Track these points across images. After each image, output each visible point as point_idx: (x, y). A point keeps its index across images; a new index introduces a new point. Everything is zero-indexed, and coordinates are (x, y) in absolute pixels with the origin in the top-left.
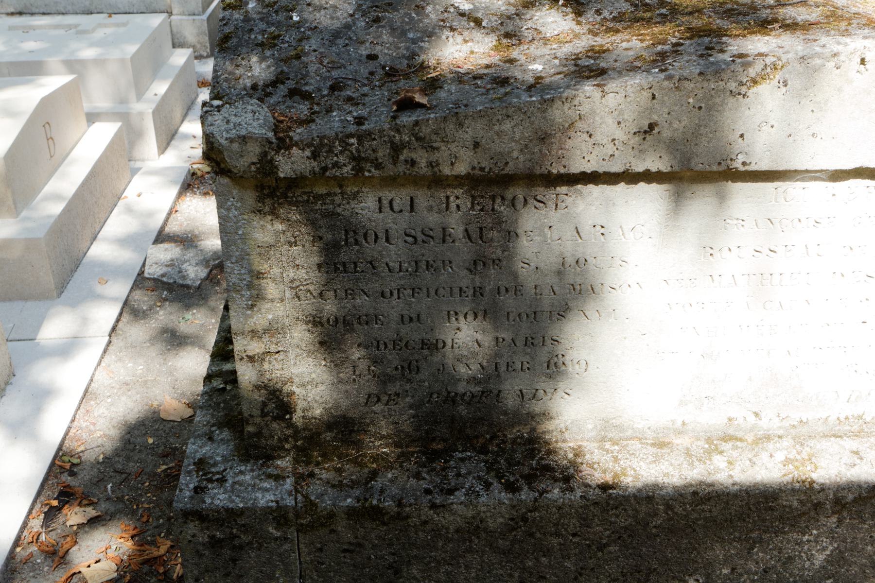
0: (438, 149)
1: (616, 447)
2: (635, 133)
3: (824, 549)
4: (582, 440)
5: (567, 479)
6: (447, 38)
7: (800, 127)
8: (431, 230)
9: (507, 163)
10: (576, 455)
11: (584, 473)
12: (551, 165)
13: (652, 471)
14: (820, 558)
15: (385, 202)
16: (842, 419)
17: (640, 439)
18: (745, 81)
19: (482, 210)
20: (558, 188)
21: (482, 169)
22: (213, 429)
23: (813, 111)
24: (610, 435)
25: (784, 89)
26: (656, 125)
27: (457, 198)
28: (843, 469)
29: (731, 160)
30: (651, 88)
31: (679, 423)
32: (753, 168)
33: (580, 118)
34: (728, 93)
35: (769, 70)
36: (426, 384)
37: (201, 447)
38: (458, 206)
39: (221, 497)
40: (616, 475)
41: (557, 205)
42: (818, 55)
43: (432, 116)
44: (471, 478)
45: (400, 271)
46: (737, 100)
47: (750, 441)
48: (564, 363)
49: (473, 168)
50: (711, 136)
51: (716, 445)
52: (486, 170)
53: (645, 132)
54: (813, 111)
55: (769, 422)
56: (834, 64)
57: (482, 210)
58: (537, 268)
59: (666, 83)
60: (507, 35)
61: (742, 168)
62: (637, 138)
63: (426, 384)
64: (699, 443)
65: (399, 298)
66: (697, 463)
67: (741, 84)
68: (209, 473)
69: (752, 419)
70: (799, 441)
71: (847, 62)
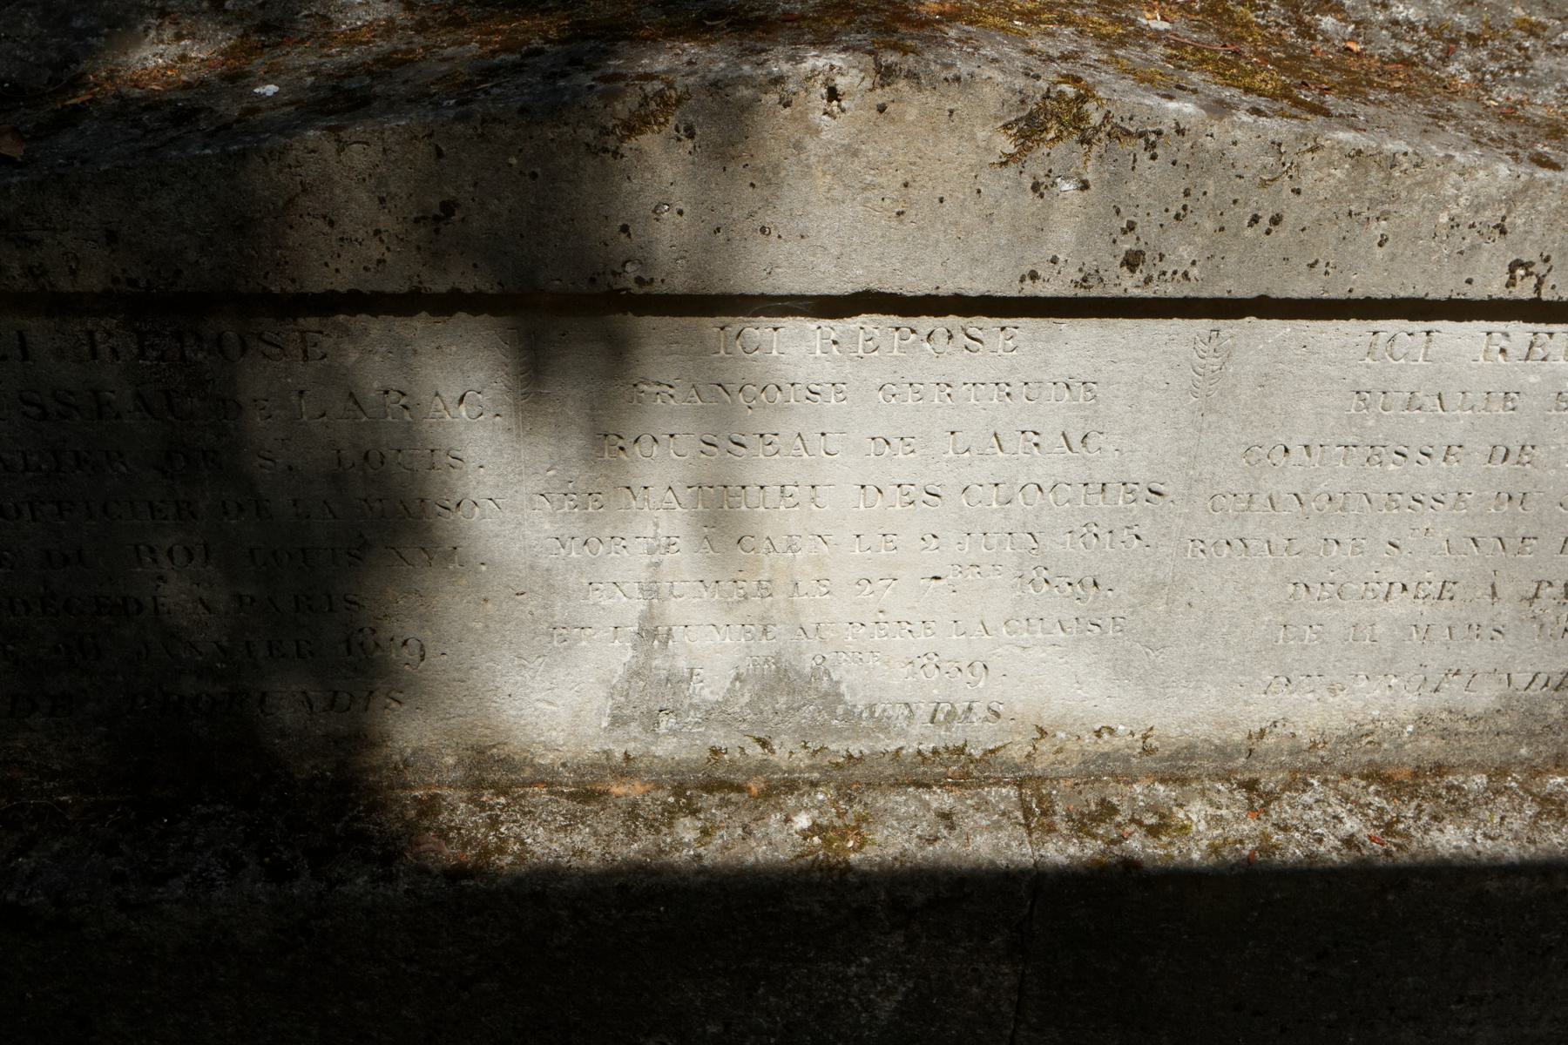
0: (39, 242)
1: (502, 800)
2: (417, 221)
3: (890, 991)
4: (440, 784)
5: (390, 857)
6: (146, 30)
7: (735, 215)
8: (71, 393)
9: (178, 272)
10: (422, 814)
11: (421, 848)
12: (265, 277)
13: (555, 846)
14: (886, 1008)
16: (929, 755)
17: (552, 784)
18: (610, 125)
19: (161, 358)
20: (301, 321)
21: (132, 282)
23: (752, 185)
24: (492, 777)
25: (689, 144)
26: (457, 206)
27: (110, 335)
28: (912, 847)
29: (614, 273)
30: (430, 136)
31: (618, 755)
32: (659, 289)
33: (304, 190)
34: (583, 148)
35: (653, 106)
36: (120, 678)
38: (114, 350)
40: (486, 852)
41: (305, 352)
42: (747, 81)
43: (15, 180)
44: (209, 854)
45: (27, 468)
46: (603, 162)
47: (755, 790)
48: (377, 645)
49: (115, 280)
50: (565, 227)
51: (689, 798)
52: (142, 284)
53: (436, 218)
54: (752, 185)
55: (787, 754)
56: (776, 97)
57: (161, 358)
58: (290, 468)
59: (459, 128)
60: (265, 28)
61: (636, 289)
62: (422, 231)
63: (120, 678)
64: (660, 794)
65: (34, 519)
66: (642, 831)
67: (605, 132)
69: (756, 751)
70: (846, 792)
71: (803, 94)
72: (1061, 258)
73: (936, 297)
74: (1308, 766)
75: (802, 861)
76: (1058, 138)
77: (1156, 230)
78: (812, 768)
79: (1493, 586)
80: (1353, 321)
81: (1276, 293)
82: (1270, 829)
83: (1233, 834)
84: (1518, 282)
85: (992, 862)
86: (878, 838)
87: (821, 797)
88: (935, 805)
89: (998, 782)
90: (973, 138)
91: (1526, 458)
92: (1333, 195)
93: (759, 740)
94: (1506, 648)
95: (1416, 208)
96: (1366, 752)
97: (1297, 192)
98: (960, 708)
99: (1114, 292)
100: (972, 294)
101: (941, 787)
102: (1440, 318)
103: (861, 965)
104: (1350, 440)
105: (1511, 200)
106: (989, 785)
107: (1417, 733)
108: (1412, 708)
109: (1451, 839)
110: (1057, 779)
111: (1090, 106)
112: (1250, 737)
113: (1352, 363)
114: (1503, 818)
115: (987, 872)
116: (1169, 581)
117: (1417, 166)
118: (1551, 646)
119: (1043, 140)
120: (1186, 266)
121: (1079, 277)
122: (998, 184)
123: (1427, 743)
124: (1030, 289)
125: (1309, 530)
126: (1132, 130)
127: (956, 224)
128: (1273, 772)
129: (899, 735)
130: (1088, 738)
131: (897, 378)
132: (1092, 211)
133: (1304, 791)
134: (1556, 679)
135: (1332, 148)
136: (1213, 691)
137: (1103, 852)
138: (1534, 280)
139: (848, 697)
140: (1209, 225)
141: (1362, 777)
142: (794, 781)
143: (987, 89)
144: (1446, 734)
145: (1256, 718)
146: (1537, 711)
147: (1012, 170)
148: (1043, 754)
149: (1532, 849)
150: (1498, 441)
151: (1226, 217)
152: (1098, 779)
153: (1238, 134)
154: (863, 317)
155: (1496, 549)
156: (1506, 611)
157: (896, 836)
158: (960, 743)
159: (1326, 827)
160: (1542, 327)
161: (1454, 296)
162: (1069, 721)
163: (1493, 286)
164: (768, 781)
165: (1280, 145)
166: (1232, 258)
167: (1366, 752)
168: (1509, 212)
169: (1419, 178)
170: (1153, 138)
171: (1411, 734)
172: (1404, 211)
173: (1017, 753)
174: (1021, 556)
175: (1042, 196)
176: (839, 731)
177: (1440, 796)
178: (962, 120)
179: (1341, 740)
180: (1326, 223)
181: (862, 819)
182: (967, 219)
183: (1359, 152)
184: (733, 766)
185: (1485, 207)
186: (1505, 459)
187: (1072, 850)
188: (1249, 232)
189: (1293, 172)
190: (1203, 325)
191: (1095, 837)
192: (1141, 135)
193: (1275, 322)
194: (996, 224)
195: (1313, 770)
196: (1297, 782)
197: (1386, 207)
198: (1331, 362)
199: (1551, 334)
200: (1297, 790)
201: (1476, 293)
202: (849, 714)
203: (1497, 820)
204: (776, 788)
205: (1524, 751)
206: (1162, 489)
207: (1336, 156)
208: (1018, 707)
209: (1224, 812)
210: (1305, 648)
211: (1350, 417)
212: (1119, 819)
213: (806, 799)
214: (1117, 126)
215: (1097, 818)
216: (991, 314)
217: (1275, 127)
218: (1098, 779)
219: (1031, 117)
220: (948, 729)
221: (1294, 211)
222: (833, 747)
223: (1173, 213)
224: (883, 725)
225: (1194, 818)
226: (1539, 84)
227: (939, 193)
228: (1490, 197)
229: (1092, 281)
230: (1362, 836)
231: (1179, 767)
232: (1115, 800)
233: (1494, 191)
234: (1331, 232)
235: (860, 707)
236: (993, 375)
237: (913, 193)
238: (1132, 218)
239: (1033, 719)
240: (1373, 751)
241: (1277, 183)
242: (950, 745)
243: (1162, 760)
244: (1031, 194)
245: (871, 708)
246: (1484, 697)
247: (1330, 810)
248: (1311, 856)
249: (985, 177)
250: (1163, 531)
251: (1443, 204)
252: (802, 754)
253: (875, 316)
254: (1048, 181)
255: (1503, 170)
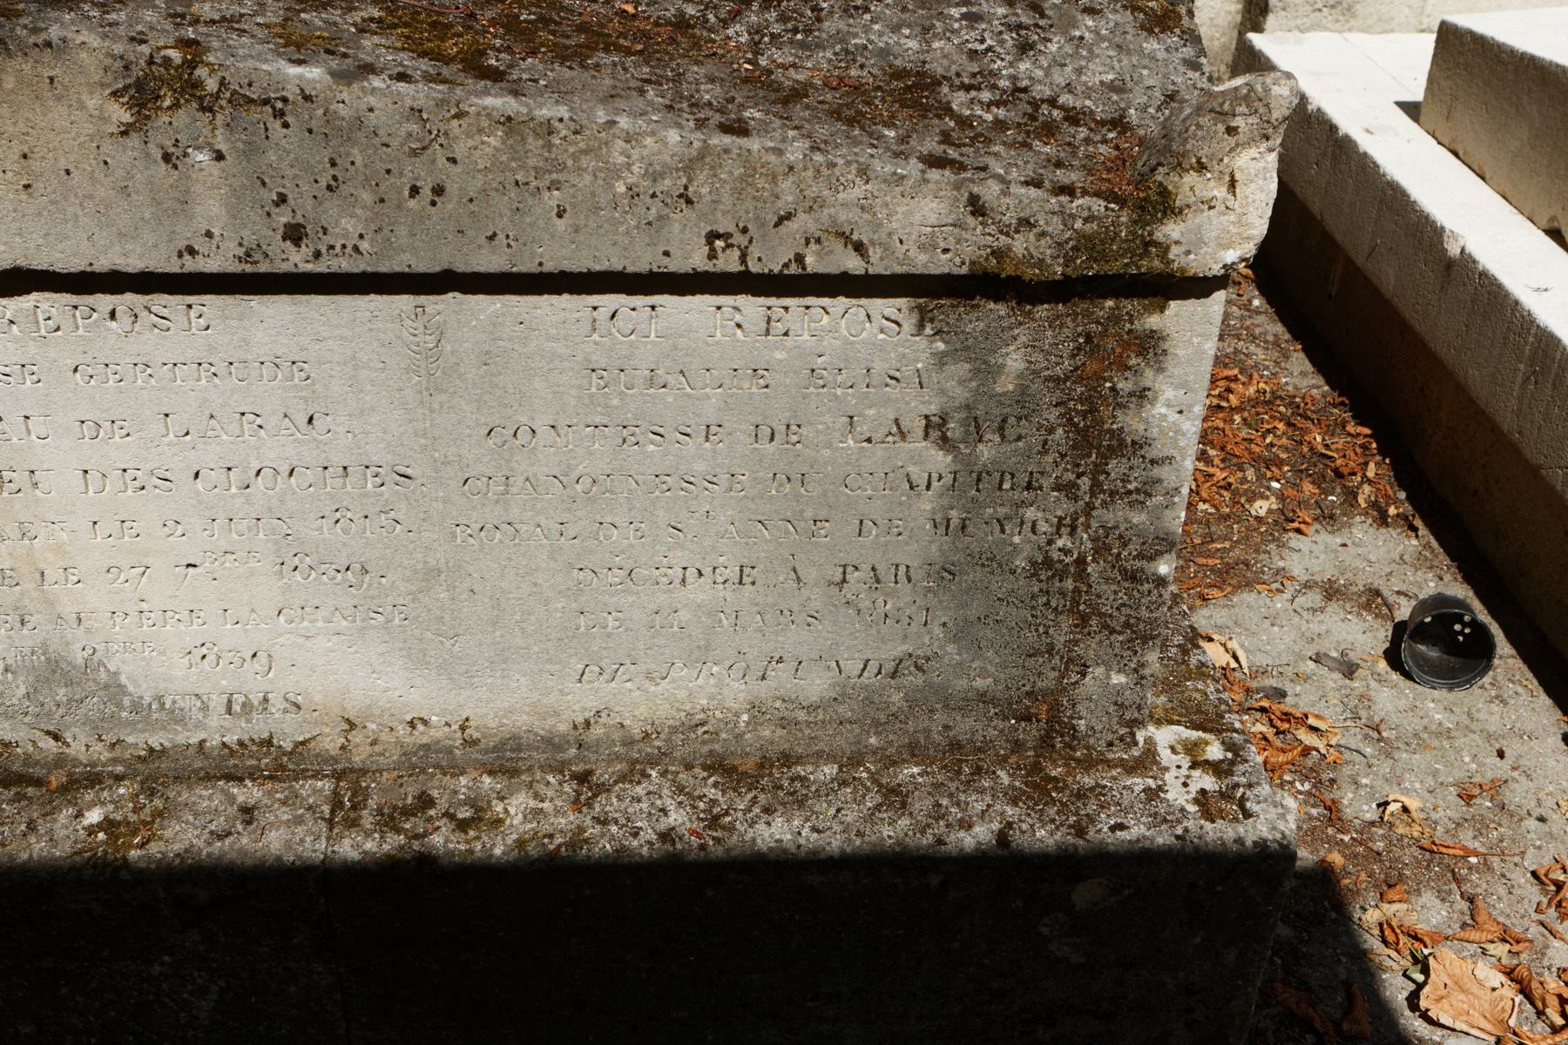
16: (236, 747)
47: (54, 784)
55: (81, 746)
69: (49, 744)
72: (216, 232)
73: (93, 274)
74: (642, 757)
75: (78, 858)
76: (176, 106)
77: (311, 202)
78: (115, 761)
79: (794, 570)
80: (566, 296)
81: (461, 267)
82: (588, 822)
83: (546, 828)
84: (720, 254)
85: (279, 858)
86: (168, 833)
87: (122, 791)
88: (241, 799)
89: (316, 775)
90: (82, 107)
91: (794, 438)
92: (493, 164)
93: (48, 733)
94: (824, 634)
95: (588, 178)
96: (704, 743)
97: (453, 161)
98: (256, 699)
99: (285, 267)
100: (130, 270)
101: (254, 780)
102: (662, 293)
103: (162, 964)
104: (597, 420)
105: (690, 166)
106: (305, 778)
107: (753, 723)
108: (741, 696)
109: (777, 832)
110: (381, 771)
111: (202, 72)
112: (575, 727)
113: (578, 340)
114: (838, 811)
115: (272, 869)
116: (442, 566)
117: (576, 132)
118: (873, 631)
119: (160, 108)
120: (355, 240)
121: (241, 252)
122: (126, 154)
123: (767, 733)
124: (191, 265)
125: (579, 513)
126: (255, 97)
127: (91, 197)
128: (609, 762)
129: (196, 727)
130: (402, 730)
131: (88, 360)
132: (236, 183)
133: (639, 783)
134: (889, 667)
135: (479, 114)
136: (523, 680)
137: (402, 847)
138: (737, 253)
139: (131, 689)
140: (367, 197)
141: (705, 767)
142: (97, 774)
143: (84, 55)
144: (784, 723)
145: (576, 707)
146: (876, 699)
147: (134, 140)
148: (357, 746)
149: (858, 843)
150: (759, 420)
151: (382, 188)
152: (423, 771)
153: (372, 100)
154: (35, 296)
155: (787, 532)
156: (816, 597)
157: (190, 831)
158: (265, 735)
159: (650, 818)
160: (772, 301)
161: (655, 270)
162: (377, 712)
163: (697, 260)
164: (70, 775)
165: (420, 111)
166: (402, 231)
167: (704, 743)
168: (690, 180)
169: (582, 145)
170: (279, 105)
171: (748, 723)
172: (574, 179)
173: (330, 743)
174: (276, 542)
175: (175, 167)
176: (132, 724)
177: (781, 787)
178: (66, 88)
179: (674, 730)
180: (493, 194)
181: (158, 814)
182: (101, 193)
183: (509, 119)
184: (27, 759)
185: (662, 176)
186: (772, 439)
187: (369, 845)
188: (412, 203)
189: (441, 140)
190: (405, 302)
191: (398, 831)
192: (266, 102)
193: (481, 297)
194: (135, 197)
195: (653, 763)
196: (634, 772)
197: (554, 176)
198: (550, 338)
199: (786, 309)
200: (631, 782)
201: (676, 265)
202: (136, 707)
203: (832, 811)
204: (78, 781)
205: (873, 740)
206: (409, 472)
207: (485, 123)
208: (318, 698)
209: (546, 805)
210: (609, 635)
211: (591, 396)
212: (432, 812)
213: (105, 793)
214: (235, 92)
215: (408, 812)
216: (172, 291)
217: (416, 93)
218: (423, 771)
219: (139, 85)
220: (248, 721)
221: (455, 180)
222: (130, 740)
223: (324, 184)
224: (177, 717)
225: (512, 811)
226: (818, 46)
227: (63, 164)
228: (664, 165)
229: (257, 256)
230: (682, 830)
231: (507, 759)
232: (435, 793)
233: (667, 158)
234: (502, 204)
235: (147, 700)
236: (191, 355)
237: (35, 164)
238: (281, 190)
239: (336, 710)
240: (712, 741)
241: (429, 151)
242: (255, 737)
243: (487, 751)
244: (163, 165)
245: (159, 699)
246: (817, 685)
247: (659, 802)
248: (621, 851)
249: (107, 146)
250: (422, 516)
251: (615, 173)
252: (99, 747)
253: (47, 295)
254: (178, 152)
255: (673, 136)
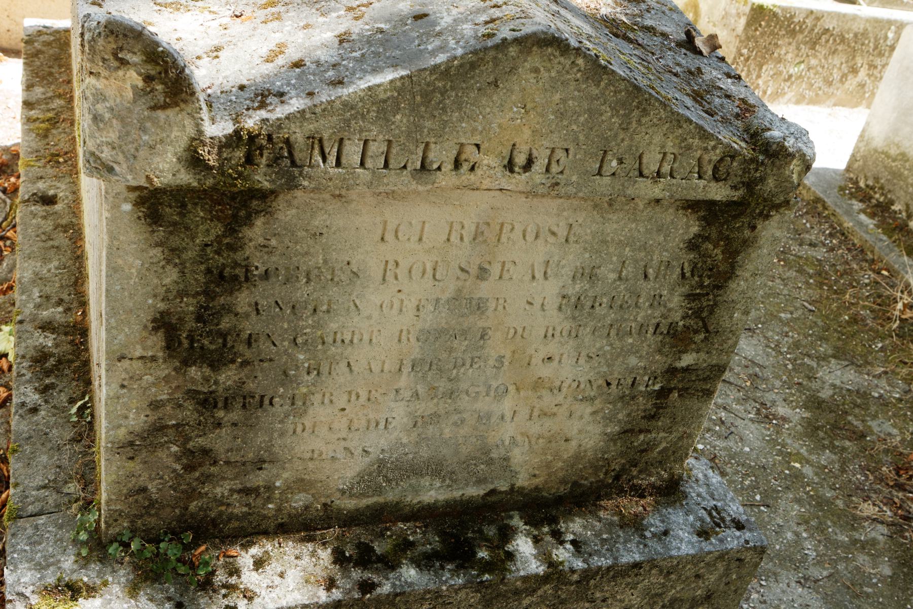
15: (391, 227)
22: (648, 534)
37: (681, 540)
39: (735, 508)
68: (714, 522)
